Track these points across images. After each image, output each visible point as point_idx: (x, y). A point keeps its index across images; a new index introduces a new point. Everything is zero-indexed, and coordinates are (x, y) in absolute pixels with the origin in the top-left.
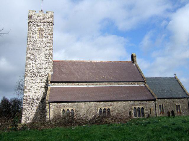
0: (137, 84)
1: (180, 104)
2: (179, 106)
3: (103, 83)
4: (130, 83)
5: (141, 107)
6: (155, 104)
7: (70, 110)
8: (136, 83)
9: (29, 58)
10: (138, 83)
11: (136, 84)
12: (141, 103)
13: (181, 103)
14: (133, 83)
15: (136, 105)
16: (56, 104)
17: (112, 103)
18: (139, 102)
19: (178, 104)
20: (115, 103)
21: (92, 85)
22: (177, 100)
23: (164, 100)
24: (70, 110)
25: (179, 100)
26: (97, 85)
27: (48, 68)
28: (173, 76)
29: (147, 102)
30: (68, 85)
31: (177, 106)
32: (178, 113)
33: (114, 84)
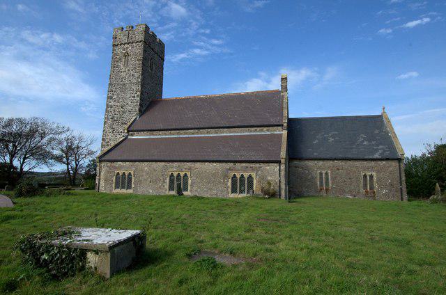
0: (268, 130)
1: (374, 174)
2: (371, 177)
3: (204, 130)
4: (253, 129)
5: (246, 175)
6: (280, 170)
7: (127, 174)
8: (265, 129)
9: (111, 98)
10: (271, 128)
11: (264, 132)
12: (247, 167)
13: (378, 172)
14: (258, 129)
15: (238, 171)
16: (109, 164)
17: (193, 166)
18: (244, 165)
19: (368, 174)
20: (198, 165)
21: (186, 134)
22: (366, 164)
23: (331, 162)
24: (127, 174)
25: (373, 163)
26: (193, 134)
27: (134, 110)
28: (378, 113)
29: (262, 165)
30: (150, 135)
31: (365, 176)
32: (367, 192)
33: (223, 132)
